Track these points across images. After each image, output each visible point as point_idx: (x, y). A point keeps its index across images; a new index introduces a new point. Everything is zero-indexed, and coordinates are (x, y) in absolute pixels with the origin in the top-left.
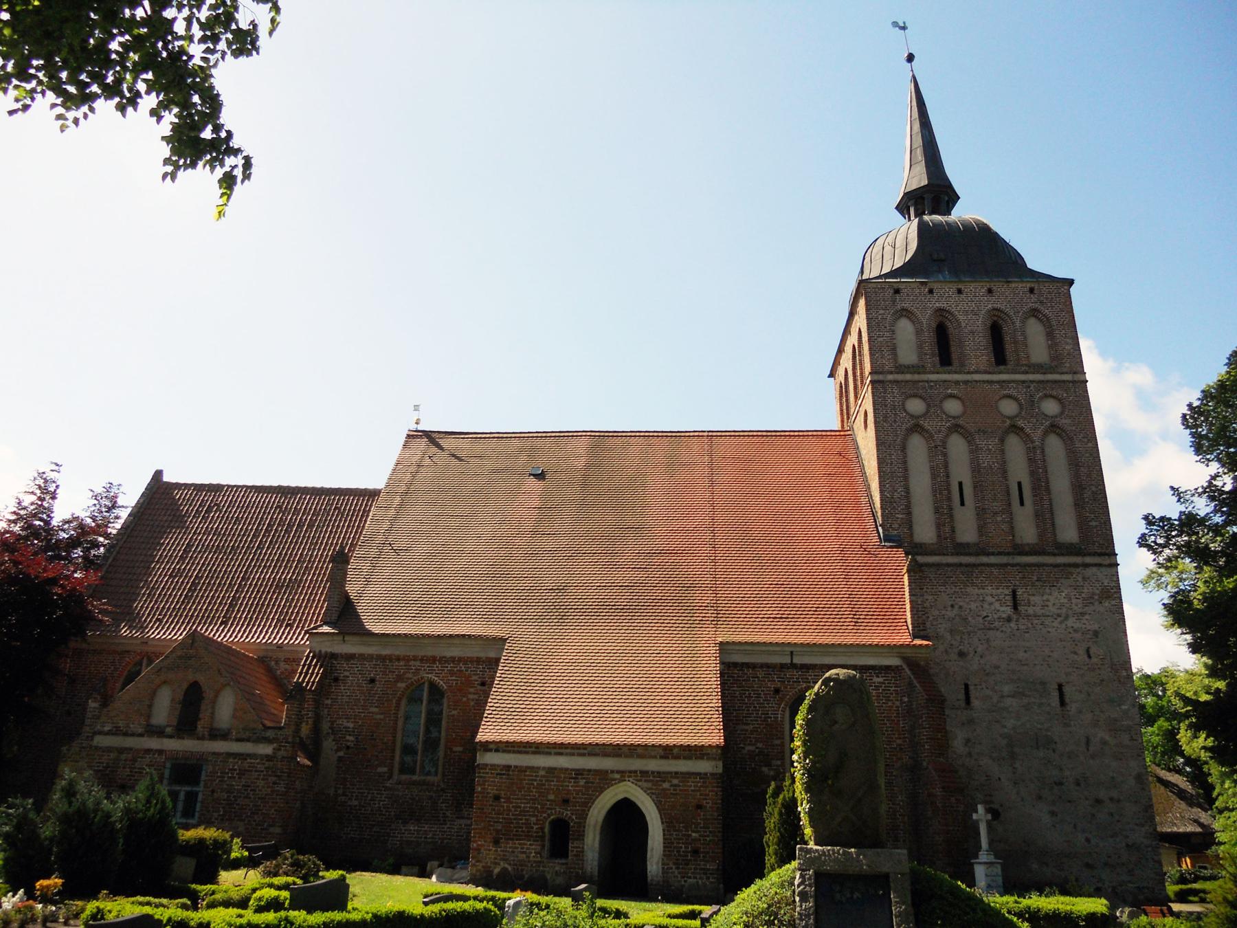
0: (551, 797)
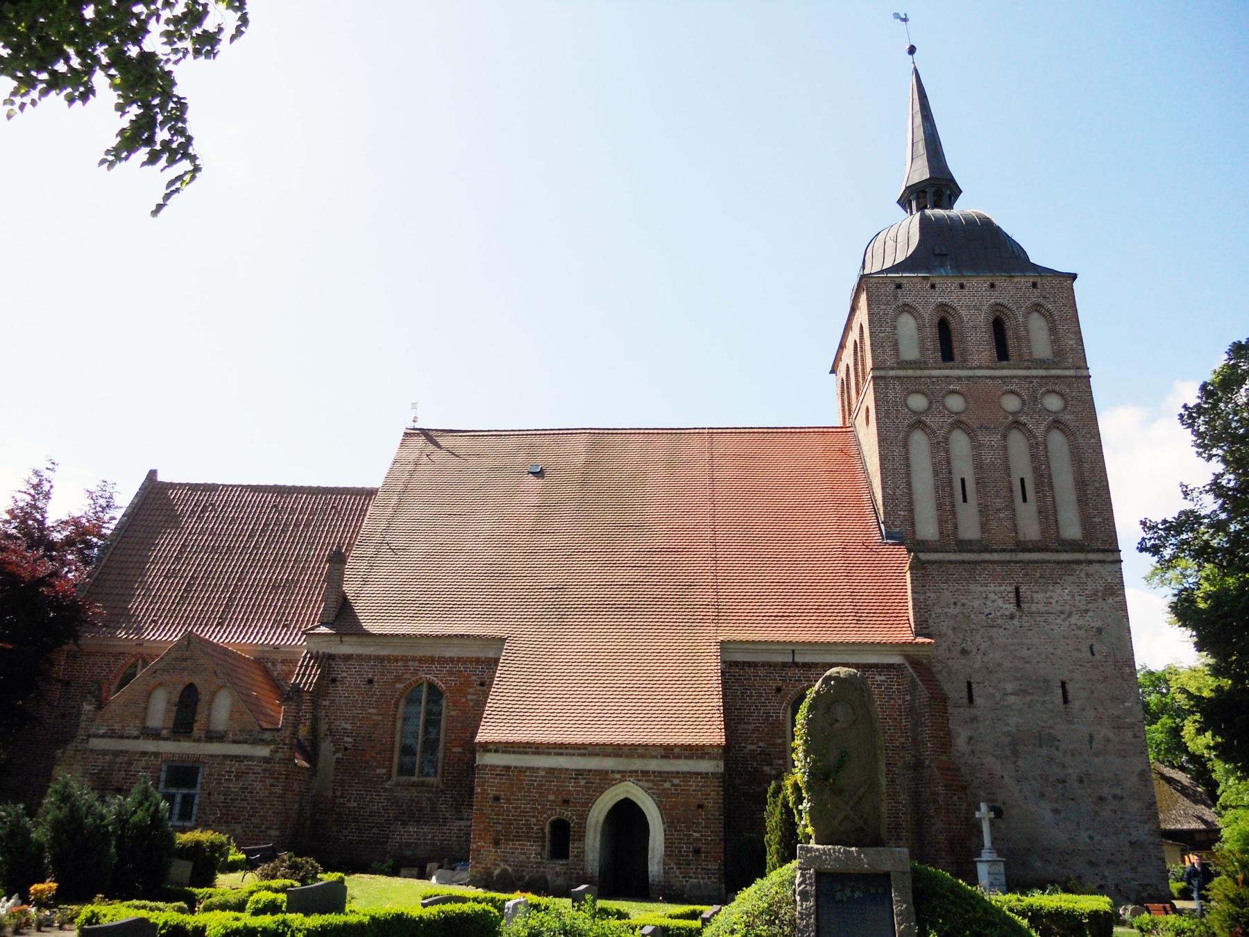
0: (551, 797)
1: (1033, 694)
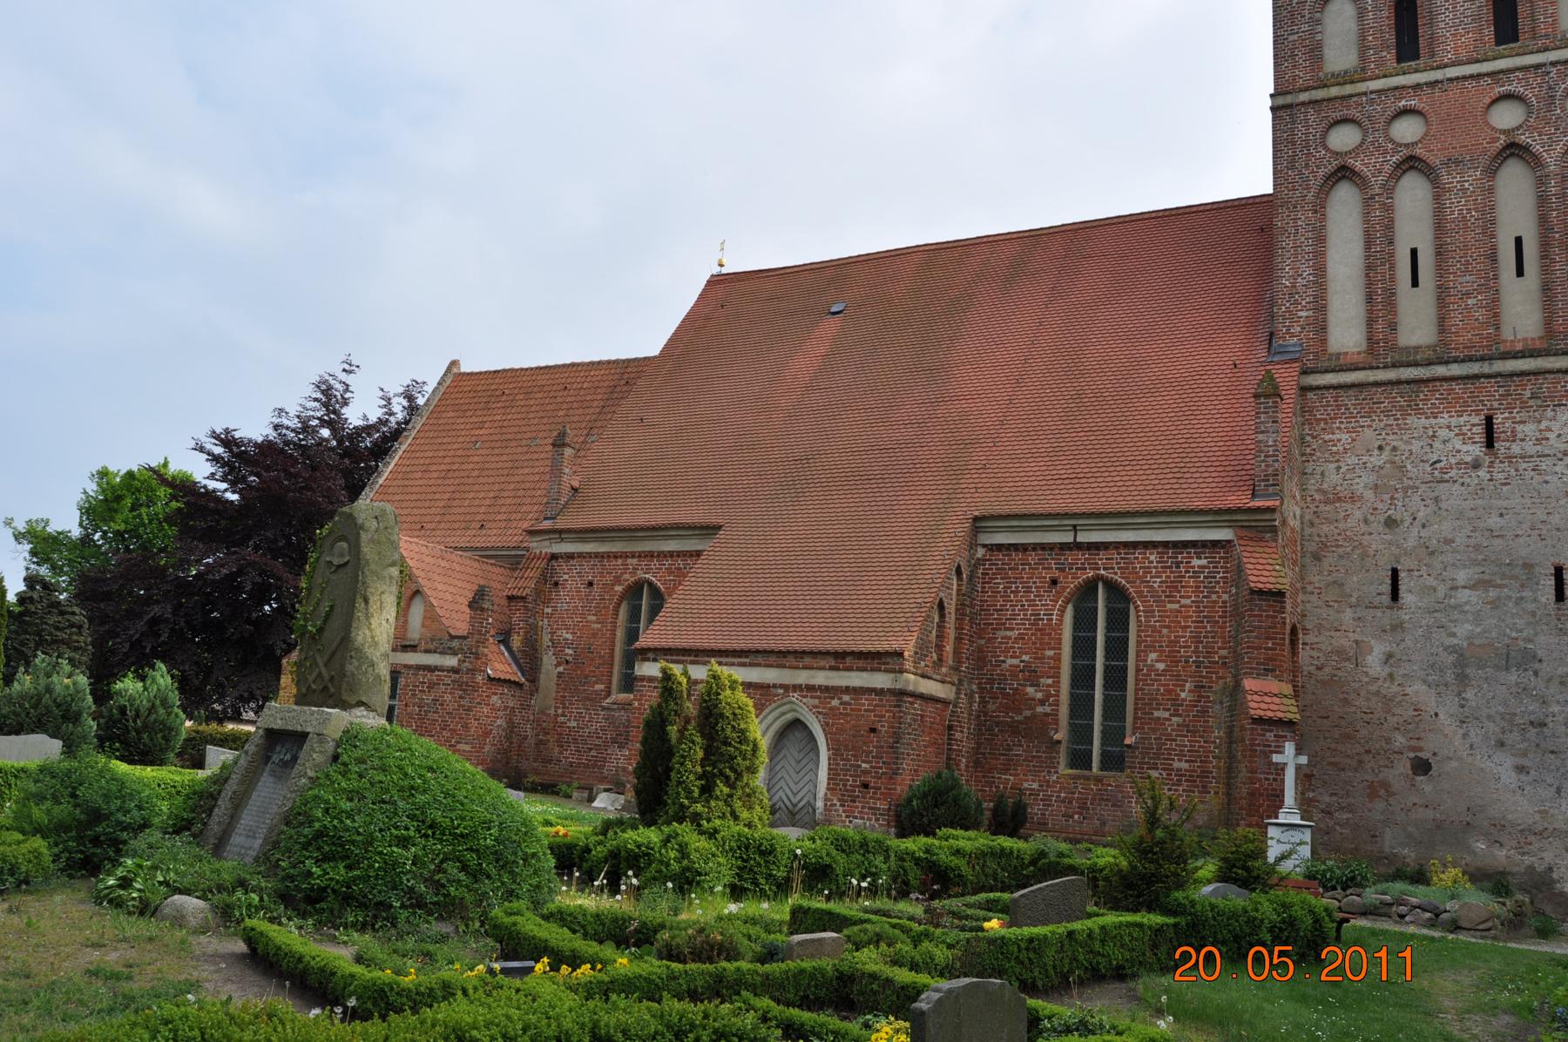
1: (1505, 586)
